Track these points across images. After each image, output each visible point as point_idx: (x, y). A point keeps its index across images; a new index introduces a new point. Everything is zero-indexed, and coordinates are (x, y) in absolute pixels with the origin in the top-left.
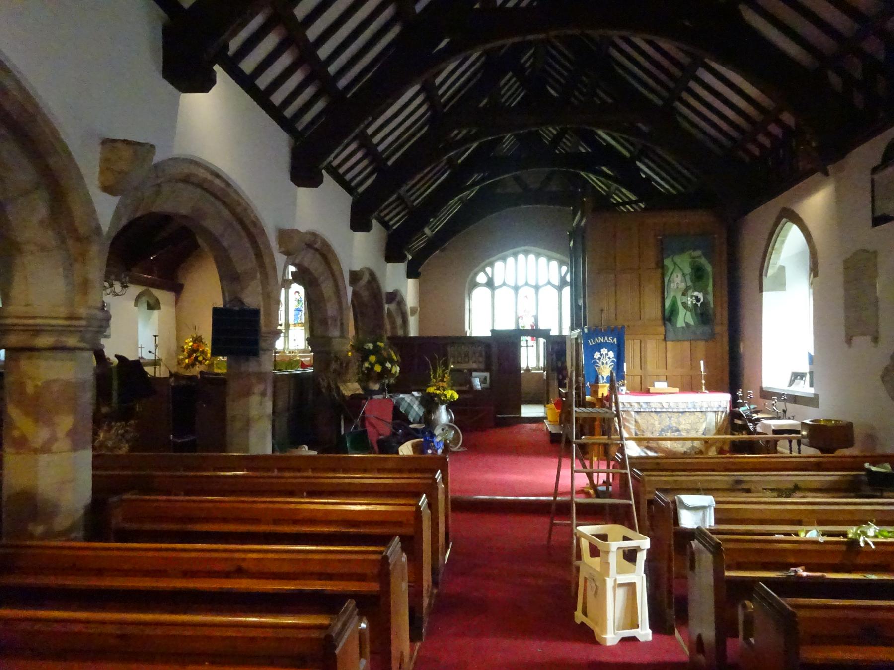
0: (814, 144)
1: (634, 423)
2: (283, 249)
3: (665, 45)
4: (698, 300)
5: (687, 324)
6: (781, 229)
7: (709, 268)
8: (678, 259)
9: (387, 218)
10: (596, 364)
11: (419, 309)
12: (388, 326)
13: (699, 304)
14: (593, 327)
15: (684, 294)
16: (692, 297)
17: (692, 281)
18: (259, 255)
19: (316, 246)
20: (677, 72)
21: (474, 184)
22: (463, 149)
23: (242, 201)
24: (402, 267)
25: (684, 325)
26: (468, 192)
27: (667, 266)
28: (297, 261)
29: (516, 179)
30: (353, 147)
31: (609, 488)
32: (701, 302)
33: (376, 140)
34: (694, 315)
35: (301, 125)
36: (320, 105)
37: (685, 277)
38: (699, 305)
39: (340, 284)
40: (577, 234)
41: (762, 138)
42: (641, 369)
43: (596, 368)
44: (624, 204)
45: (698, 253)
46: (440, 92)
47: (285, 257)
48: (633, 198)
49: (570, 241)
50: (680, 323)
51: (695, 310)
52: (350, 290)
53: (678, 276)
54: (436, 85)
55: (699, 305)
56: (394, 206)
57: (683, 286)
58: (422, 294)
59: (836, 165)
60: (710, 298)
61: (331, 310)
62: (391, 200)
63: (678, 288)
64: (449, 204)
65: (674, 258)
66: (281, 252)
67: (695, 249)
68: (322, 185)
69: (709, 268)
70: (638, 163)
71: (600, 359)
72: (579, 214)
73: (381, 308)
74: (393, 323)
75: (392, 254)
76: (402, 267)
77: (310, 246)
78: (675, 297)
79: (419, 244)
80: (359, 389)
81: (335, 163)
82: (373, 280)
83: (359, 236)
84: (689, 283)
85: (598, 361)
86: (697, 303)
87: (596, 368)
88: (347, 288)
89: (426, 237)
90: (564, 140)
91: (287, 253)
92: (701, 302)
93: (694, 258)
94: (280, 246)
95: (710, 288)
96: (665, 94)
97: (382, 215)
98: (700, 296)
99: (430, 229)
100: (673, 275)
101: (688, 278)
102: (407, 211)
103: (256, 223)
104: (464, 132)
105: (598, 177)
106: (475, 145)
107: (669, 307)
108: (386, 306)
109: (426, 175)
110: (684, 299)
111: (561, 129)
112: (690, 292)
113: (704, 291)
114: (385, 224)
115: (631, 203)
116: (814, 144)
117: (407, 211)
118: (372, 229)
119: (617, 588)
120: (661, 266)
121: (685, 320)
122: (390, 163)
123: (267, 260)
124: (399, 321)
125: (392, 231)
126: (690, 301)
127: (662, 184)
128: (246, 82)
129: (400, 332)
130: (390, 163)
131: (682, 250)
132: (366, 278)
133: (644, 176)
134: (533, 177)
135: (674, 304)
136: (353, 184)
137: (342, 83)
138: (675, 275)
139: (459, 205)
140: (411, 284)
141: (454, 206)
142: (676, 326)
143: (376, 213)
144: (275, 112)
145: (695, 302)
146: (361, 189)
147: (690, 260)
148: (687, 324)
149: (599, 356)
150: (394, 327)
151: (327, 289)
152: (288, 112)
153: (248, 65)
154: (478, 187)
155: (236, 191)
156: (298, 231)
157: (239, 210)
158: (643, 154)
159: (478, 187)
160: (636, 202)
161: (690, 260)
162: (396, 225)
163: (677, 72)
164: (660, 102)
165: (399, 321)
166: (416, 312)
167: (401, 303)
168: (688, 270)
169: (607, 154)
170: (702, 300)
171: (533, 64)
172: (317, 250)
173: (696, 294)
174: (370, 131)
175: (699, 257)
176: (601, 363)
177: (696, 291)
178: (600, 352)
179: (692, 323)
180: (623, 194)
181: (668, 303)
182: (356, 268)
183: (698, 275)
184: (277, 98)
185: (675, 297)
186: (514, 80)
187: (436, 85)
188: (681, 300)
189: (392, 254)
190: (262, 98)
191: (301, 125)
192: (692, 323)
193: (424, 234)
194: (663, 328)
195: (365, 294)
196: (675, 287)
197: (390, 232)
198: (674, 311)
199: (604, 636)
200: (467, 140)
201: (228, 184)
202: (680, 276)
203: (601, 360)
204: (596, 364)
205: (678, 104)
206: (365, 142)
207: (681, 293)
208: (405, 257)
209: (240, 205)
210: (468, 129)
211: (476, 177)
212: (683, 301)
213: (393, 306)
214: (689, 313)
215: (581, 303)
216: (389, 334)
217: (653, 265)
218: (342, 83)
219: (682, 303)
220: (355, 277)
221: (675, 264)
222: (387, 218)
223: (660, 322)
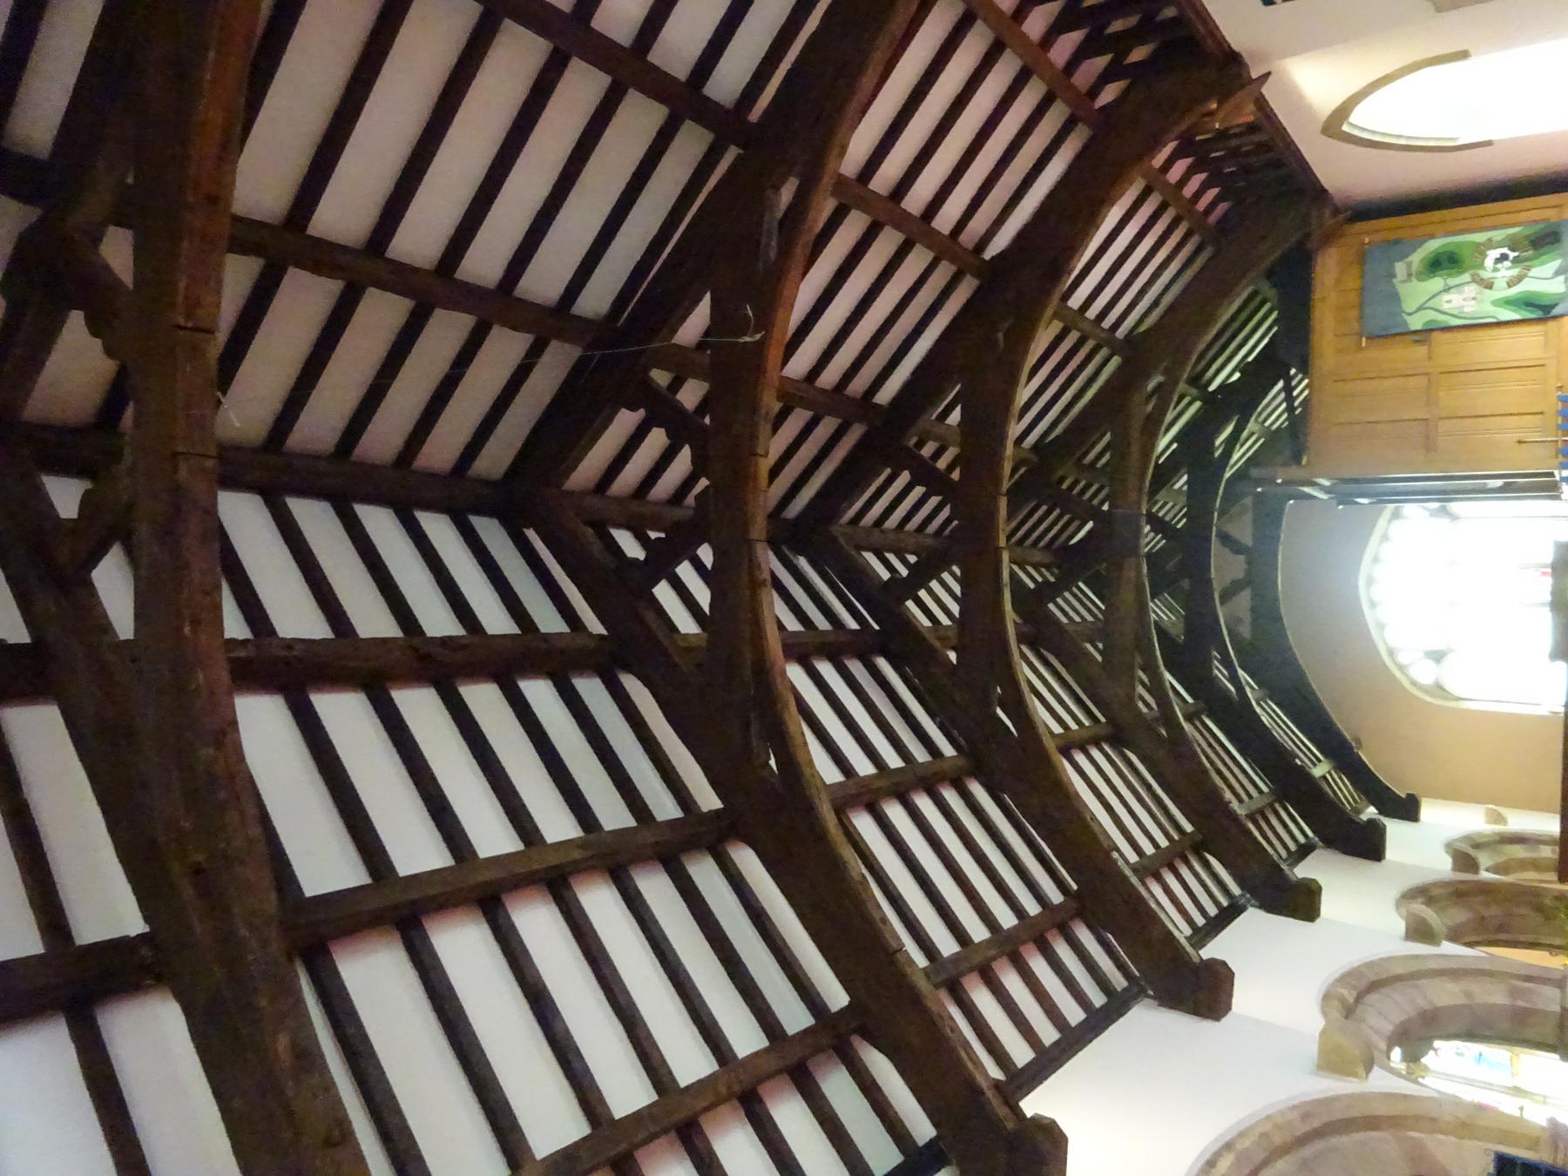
0: (1214, 106)
2: (1361, 1071)
3: (1032, 360)
4: (1504, 257)
5: (1557, 273)
6: (1363, 129)
7: (1433, 245)
8: (1409, 305)
9: (1293, 847)
11: (1490, 806)
12: (1529, 877)
13: (1512, 255)
14: (1561, 459)
16: (1495, 270)
18: (1372, 1123)
19: (1351, 1000)
20: (1073, 337)
21: (1234, 679)
22: (1171, 694)
23: (1260, 1130)
24: (1395, 830)
25: (1561, 278)
26: (1248, 690)
27: (1424, 324)
28: (1383, 1045)
29: (1226, 596)
30: (1157, 890)
33: (1149, 849)
35: (1119, 982)
36: (1084, 935)
37: (1450, 288)
38: (1516, 254)
39: (1433, 965)
40: (1347, 489)
41: (1175, 174)
42: (1463, 55)
44: (1290, 399)
45: (1400, 268)
46: (1074, 726)
47: (1376, 1070)
48: (1281, 384)
49: (1357, 503)
50: (1556, 287)
51: (1527, 259)
52: (1449, 948)
53: (1449, 302)
55: (1516, 254)
56: (1264, 825)
57: (1472, 290)
58: (1455, 793)
59: (1250, 65)
60: (1498, 235)
61: (1495, 996)
62: (1256, 834)
63: (1474, 299)
64: (1270, 726)
65: (1411, 311)
66: (1367, 1077)
67: (1393, 275)
68: (1230, 965)
69: (1433, 245)
70: (1212, 388)
72: (1306, 490)
73: (1486, 889)
74: (1524, 865)
75: (1368, 846)
76: (1395, 830)
77: (1349, 1012)
78: (1496, 303)
79: (1343, 790)
81: (1188, 931)
82: (1424, 893)
83: (1328, 905)
84: (1466, 277)
88: (1445, 953)
89: (1331, 775)
90: (1160, 514)
91: (1369, 1066)
93: (1409, 275)
94: (1353, 1074)
95: (1480, 237)
96: (1104, 352)
97: (1284, 853)
98: (1494, 254)
99: (1315, 765)
100: (1446, 311)
101: (1452, 281)
102: (1277, 806)
103: (1307, 1110)
104: (1140, 690)
105: (1175, 399)
106: (1168, 676)
107: (1515, 311)
108: (1485, 875)
109: (1212, 763)
110: (1500, 283)
111: (1147, 523)
112: (1486, 274)
113: (1481, 250)
114: (1304, 851)
115: (1288, 389)
116: (1214, 106)
117: (1277, 806)
118: (1314, 880)
120: (1425, 335)
121: (1552, 278)
122: (1188, 828)
123: (1381, 1110)
124: (1518, 852)
125: (1317, 839)
126: (1507, 271)
127: (1254, 345)
128: (1048, 1061)
129: (1549, 853)
130: (1188, 828)
131: (1395, 298)
132: (1419, 908)
133: (1237, 375)
134: (1224, 567)
135: (1509, 303)
136: (1225, 903)
137: (1056, 897)
138: (1446, 307)
139: (1267, 704)
140: (1429, 810)
141: (1270, 715)
142: (1564, 293)
143: (1284, 867)
144: (1098, 1022)
145: (1507, 264)
146: (1235, 890)
147: (1415, 281)
148: (1557, 273)
150: (1535, 865)
151: (1445, 994)
152: (1098, 999)
153: (1021, 1054)
154: (1241, 672)
155: (1241, 1135)
156: (1323, 1033)
157: (1278, 1139)
158: (1197, 381)
159: (1241, 672)
160: (1288, 379)
161: (1415, 281)
162: (1302, 831)
163: (1073, 337)
164: (1115, 361)
165: (1518, 852)
166: (1499, 814)
167: (1478, 843)
168: (1436, 283)
169: (1196, 438)
170: (1505, 250)
171: (1036, 567)
172: (1359, 998)
173: (1489, 262)
174: (1133, 857)
175: (1409, 265)
177: (1483, 263)
180: (1273, 411)
182: (1401, 926)
183: (1444, 263)
184: (1074, 1014)
185: (1496, 303)
186: (1059, 600)
188: (1504, 289)
189: (1368, 846)
190: (1073, 1040)
191: (1119, 982)
193: (1324, 777)
195: (1459, 915)
196: (1473, 302)
197: (1321, 844)
198: (1527, 302)
200: (1157, 688)
201: (1228, 1146)
202: (1446, 297)
205: (1121, 333)
206: (1151, 869)
207: (1487, 291)
208: (1372, 823)
209: (1264, 1135)
210: (1137, 683)
211: (1220, 672)
212: (1505, 285)
213: (1484, 859)
214: (1534, 272)
215: (1499, 483)
216: (1553, 876)
217: (1421, 351)
218: (1056, 897)
219: (1510, 286)
220: (1419, 931)
221: (1420, 308)
222: (1293, 847)
223: (1552, 325)
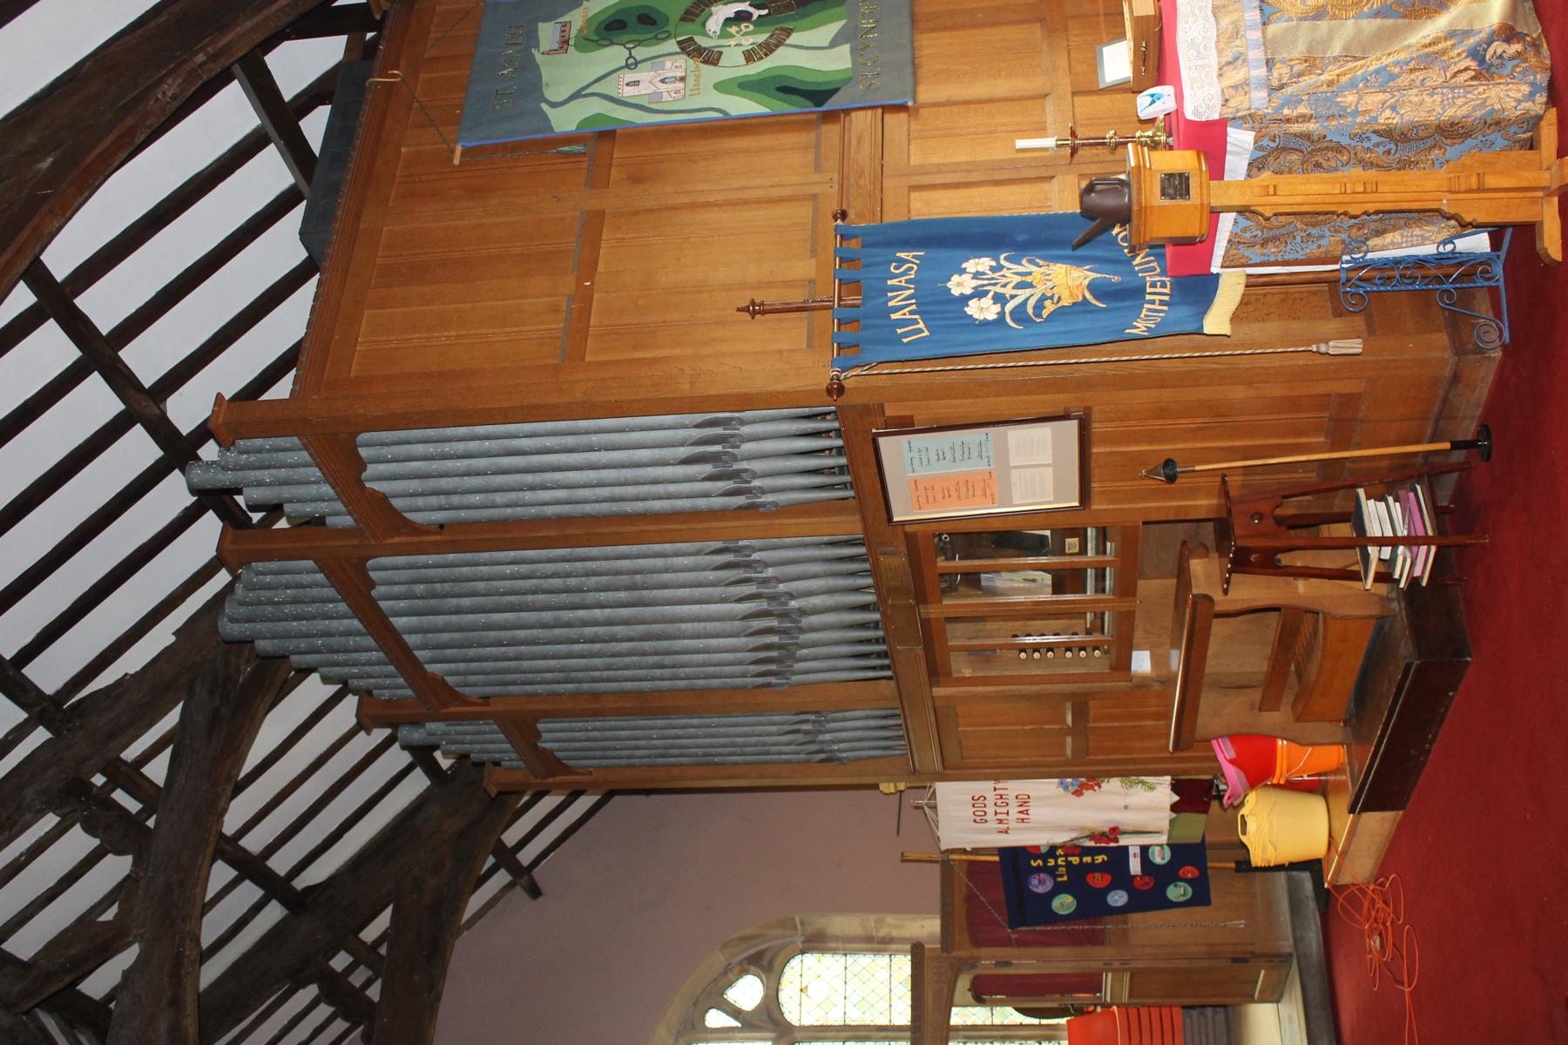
1: (1324, 25)
10: (1030, 311)
13: (756, 13)
15: (711, 58)
17: (657, 40)
31: (1167, 658)
32: (751, 10)
34: (803, 23)
37: (637, 63)
43: (1045, 313)
50: (838, 61)
54: (235, 497)
57: (678, 65)
71: (999, 299)
80: (877, 931)
85: (1009, 307)
86: (755, 17)
87: (1045, 313)
92: (751, 10)
119: (1353, 510)
135: (746, 86)
149: (987, 302)
176: (1023, 294)
178: (965, 299)
179: (834, 28)
181: (743, 106)
187: (235, 497)
192: (834, 28)
194: (854, 115)
198: (785, 87)
199: (195, 498)
203: (1008, 291)
204: (1030, 311)
223: (831, 131)
